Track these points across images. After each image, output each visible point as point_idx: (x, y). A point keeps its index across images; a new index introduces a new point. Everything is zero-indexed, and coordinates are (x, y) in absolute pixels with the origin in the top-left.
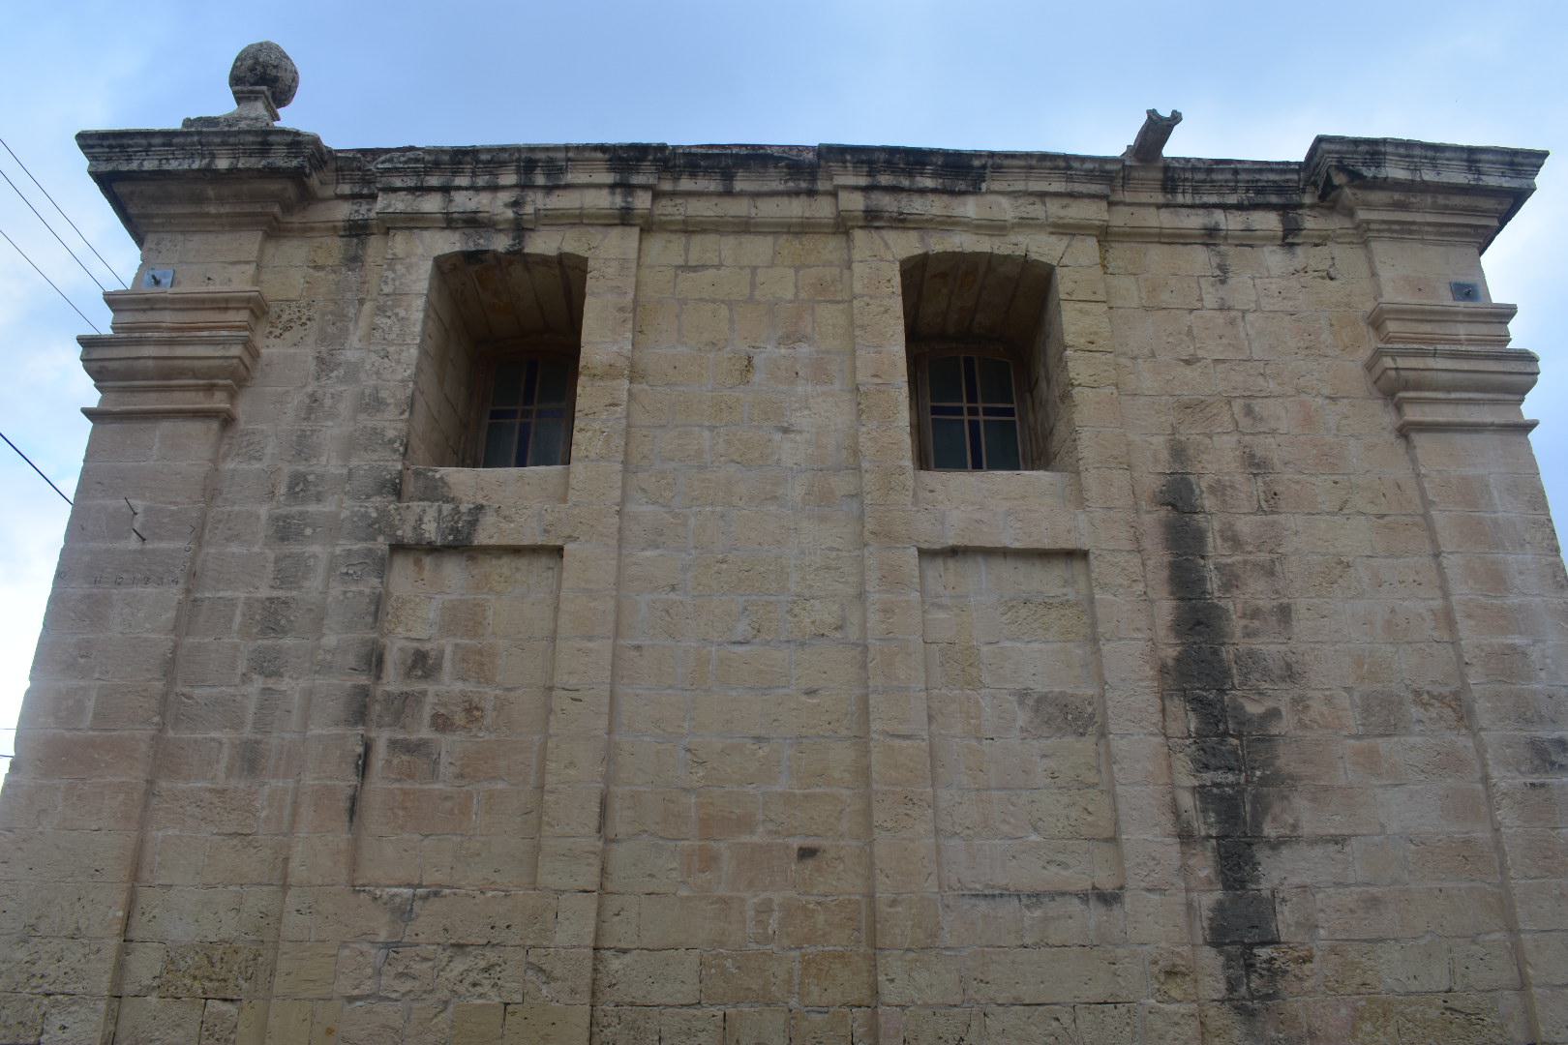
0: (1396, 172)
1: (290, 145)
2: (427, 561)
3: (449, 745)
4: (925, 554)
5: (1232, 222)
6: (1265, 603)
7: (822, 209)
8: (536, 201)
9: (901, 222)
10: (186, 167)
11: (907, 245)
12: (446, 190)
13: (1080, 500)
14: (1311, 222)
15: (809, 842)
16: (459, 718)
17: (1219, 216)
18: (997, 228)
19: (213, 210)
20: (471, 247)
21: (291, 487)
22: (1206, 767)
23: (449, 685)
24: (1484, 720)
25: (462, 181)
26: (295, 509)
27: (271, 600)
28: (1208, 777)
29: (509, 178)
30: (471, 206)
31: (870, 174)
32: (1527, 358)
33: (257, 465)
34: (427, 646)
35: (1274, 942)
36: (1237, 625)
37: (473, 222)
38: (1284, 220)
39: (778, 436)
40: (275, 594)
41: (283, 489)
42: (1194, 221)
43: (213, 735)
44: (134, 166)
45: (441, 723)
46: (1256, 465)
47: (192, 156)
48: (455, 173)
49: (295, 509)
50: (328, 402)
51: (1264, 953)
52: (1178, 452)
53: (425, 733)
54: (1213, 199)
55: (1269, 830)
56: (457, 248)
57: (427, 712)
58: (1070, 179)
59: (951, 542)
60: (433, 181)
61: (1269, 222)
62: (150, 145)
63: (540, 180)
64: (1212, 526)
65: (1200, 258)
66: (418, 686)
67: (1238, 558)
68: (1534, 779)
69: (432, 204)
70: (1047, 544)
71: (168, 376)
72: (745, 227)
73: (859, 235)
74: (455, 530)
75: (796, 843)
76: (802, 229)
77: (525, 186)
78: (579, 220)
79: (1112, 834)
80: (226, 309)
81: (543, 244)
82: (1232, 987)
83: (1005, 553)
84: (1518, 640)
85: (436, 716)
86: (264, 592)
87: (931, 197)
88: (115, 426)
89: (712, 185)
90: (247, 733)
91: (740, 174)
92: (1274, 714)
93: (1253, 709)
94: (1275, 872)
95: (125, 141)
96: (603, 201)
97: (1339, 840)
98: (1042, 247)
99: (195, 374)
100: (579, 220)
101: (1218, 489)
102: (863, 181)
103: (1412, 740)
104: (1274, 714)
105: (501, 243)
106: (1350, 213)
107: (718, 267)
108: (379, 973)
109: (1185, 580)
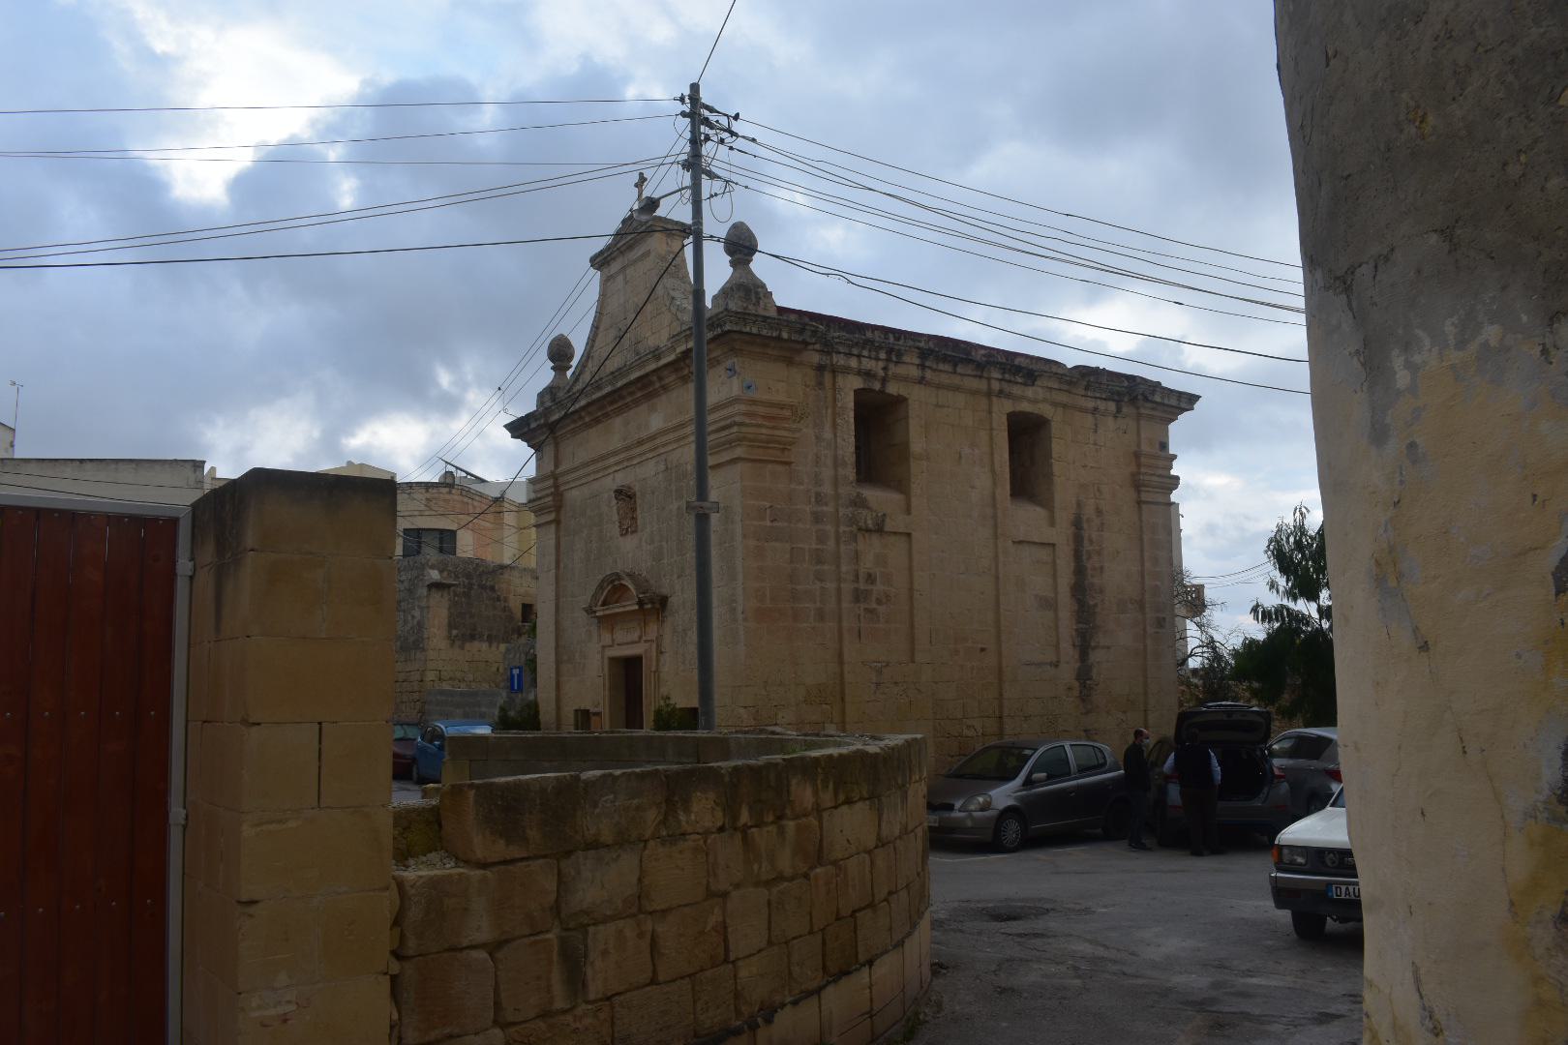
0: (1157, 398)
1: (813, 331)
2: (867, 535)
3: (881, 609)
4: (1014, 542)
5: (1102, 405)
6: (1097, 565)
7: (982, 385)
8: (893, 369)
9: (1009, 396)
10: (769, 334)
11: (1008, 406)
12: (859, 356)
13: (1052, 523)
14: (1125, 410)
15: (983, 646)
16: (884, 600)
17: (1099, 402)
18: (1035, 401)
19: (770, 352)
20: (866, 387)
21: (816, 498)
22: (1080, 623)
23: (879, 587)
24: (1147, 610)
25: (865, 353)
26: (819, 509)
27: (817, 549)
28: (1081, 625)
29: (883, 355)
30: (869, 367)
31: (1004, 373)
32: (1177, 478)
33: (802, 487)
34: (870, 571)
35: (1090, 679)
36: (1089, 572)
37: (868, 375)
38: (1117, 405)
39: (970, 489)
40: (818, 547)
41: (813, 500)
42: (1090, 404)
43: (807, 605)
44: (748, 329)
45: (879, 602)
46: (1099, 512)
47: (771, 328)
48: (863, 348)
49: (819, 509)
50: (823, 458)
51: (1088, 682)
52: (1079, 505)
53: (874, 606)
54: (1098, 395)
55: (1093, 644)
56: (862, 386)
57: (874, 599)
58: (1061, 383)
59: (1021, 539)
60: (855, 351)
61: (1112, 406)
62: (757, 321)
63: (894, 359)
64: (1086, 535)
65: (1089, 419)
66: (870, 587)
67: (1091, 548)
68: (1157, 630)
69: (853, 363)
70: (1046, 541)
71: (768, 442)
72: (957, 389)
73: (994, 399)
74: (878, 525)
75: (980, 646)
76: (974, 393)
77: (888, 360)
78: (905, 379)
79: (499, 955)
80: (782, 408)
81: (893, 389)
82: (1081, 692)
83: (1035, 543)
84: (1158, 583)
85: (877, 599)
86: (814, 546)
87: (1019, 386)
88: (750, 464)
89: (948, 367)
90: (818, 605)
91: (960, 366)
92: (1096, 605)
93: (1091, 603)
94: (1095, 656)
95: (747, 317)
96: (915, 372)
97: (1108, 648)
98: (1045, 410)
99: (779, 443)
100: (905, 379)
101: (1088, 520)
102: (1000, 377)
103: (1128, 615)
104: (1096, 605)
105: (877, 386)
106: (1138, 408)
107: (948, 407)
108: (875, 693)
109: (1077, 555)
